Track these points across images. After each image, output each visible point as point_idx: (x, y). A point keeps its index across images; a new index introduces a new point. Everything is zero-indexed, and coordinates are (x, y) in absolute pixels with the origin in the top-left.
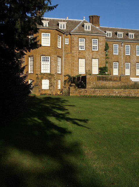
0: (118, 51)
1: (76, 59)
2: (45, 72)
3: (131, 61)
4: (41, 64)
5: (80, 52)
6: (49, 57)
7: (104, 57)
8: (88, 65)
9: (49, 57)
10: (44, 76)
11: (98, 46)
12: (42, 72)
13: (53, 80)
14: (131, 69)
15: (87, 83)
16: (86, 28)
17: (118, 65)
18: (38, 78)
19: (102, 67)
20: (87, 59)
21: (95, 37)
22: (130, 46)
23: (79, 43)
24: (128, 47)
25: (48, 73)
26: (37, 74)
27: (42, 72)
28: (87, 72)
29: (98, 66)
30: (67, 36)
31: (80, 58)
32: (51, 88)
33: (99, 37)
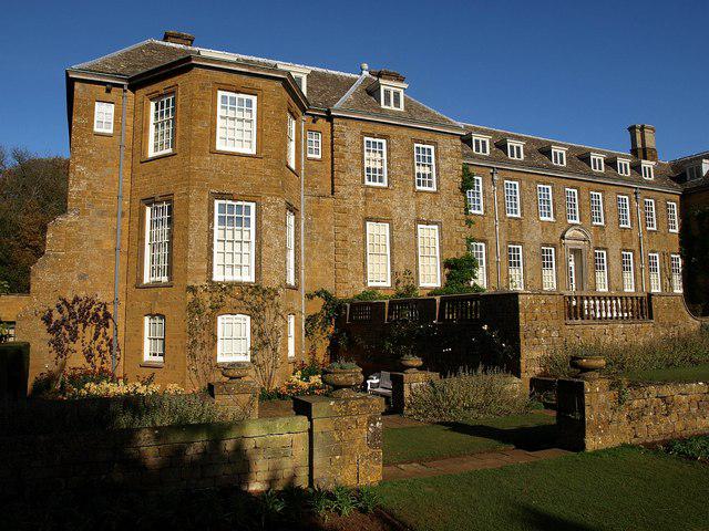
0: (518, 199)
1: (354, 225)
2: (229, 278)
3: (526, 238)
4: (211, 238)
5: (368, 194)
6: (253, 205)
7: (460, 216)
8: (403, 248)
9: (253, 205)
10: (228, 299)
11: (437, 175)
12: (218, 277)
13: (269, 315)
14: (528, 267)
15: (521, 338)
16: (387, 102)
17: (484, 252)
18: (194, 308)
19: (453, 255)
21: (426, 136)
22: (517, 183)
23: (366, 154)
24: (513, 189)
25: (248, 285)
26: (192, 289)
27: (218, 277)
28: (401, 277)
29: (438, 255)
30: (314, 122)
31: (371, 220)
32: (260, 358)
33: (439, 139)
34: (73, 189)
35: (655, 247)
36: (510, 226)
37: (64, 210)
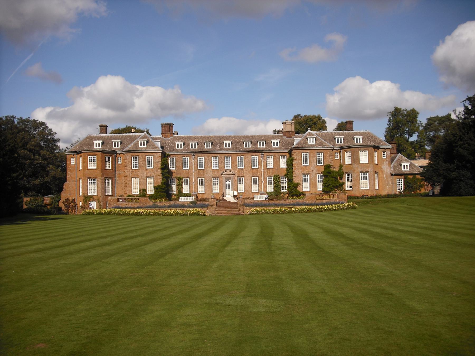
1: (129, 179)
3: (206, 175)
20: (140, 177)
21: (149, 154)
34: (68, 177)
35: (271, 174)
36: (199, 172)
37: (66, 181)
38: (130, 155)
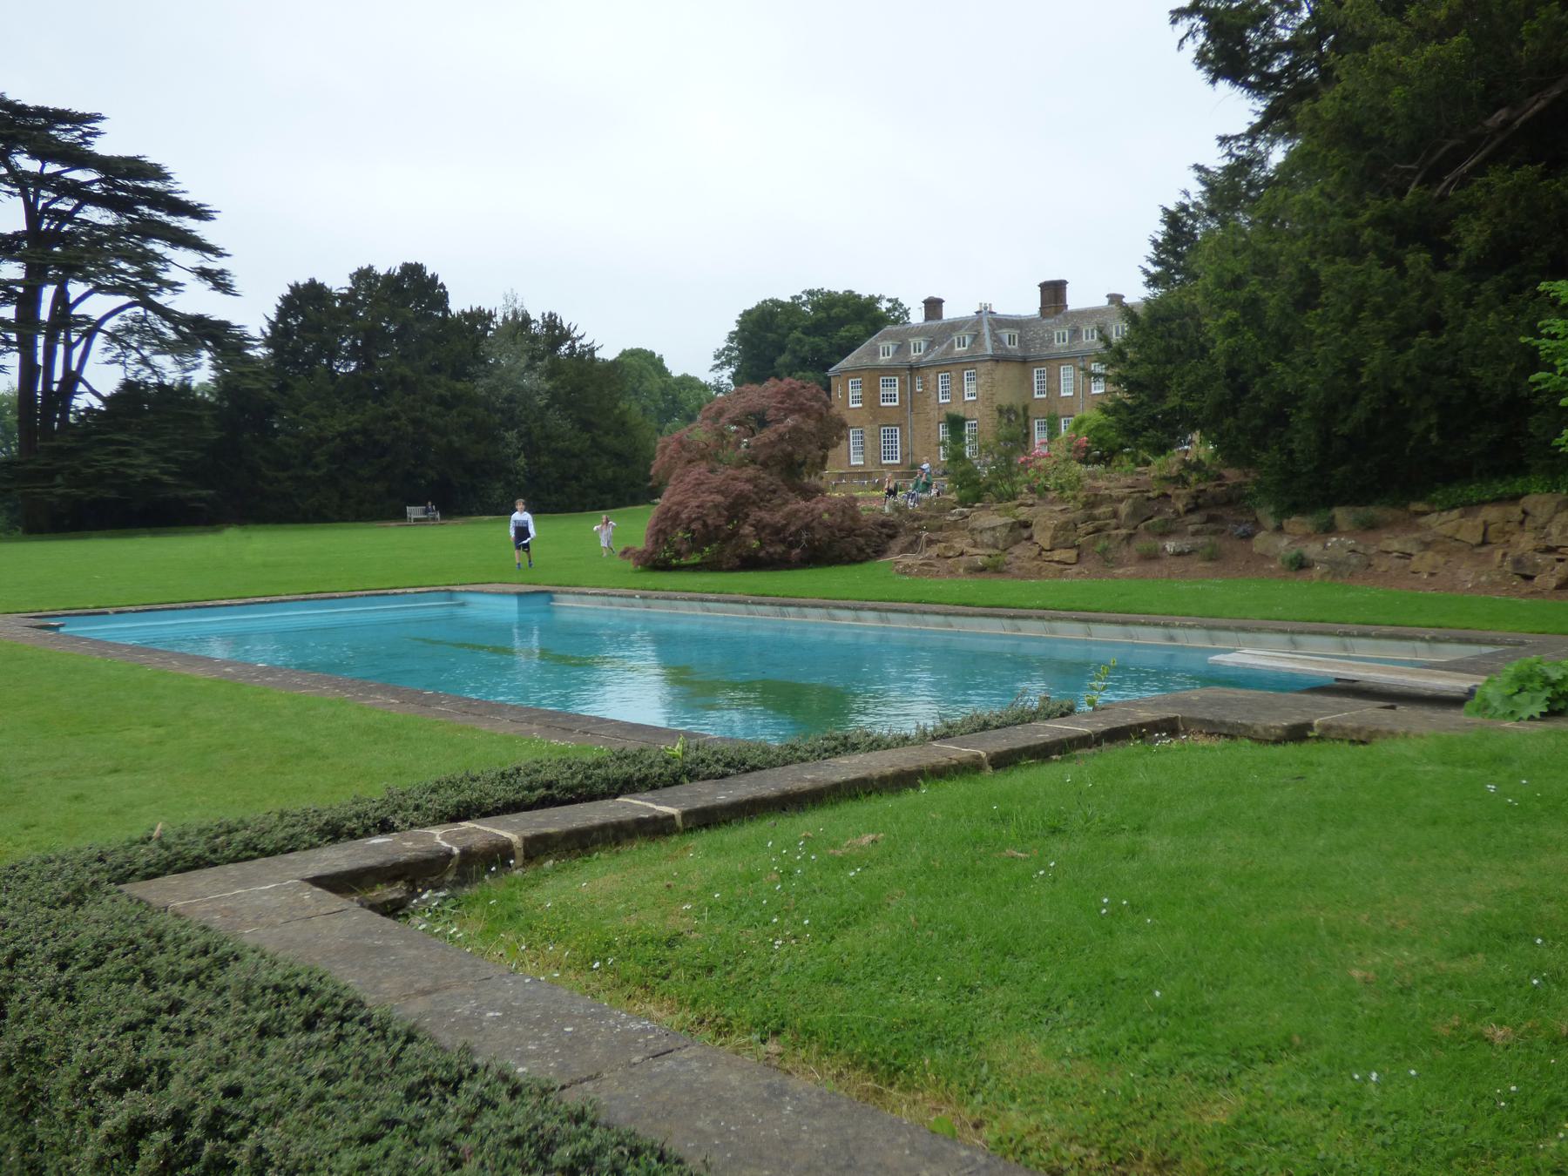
38: (934, 371)
